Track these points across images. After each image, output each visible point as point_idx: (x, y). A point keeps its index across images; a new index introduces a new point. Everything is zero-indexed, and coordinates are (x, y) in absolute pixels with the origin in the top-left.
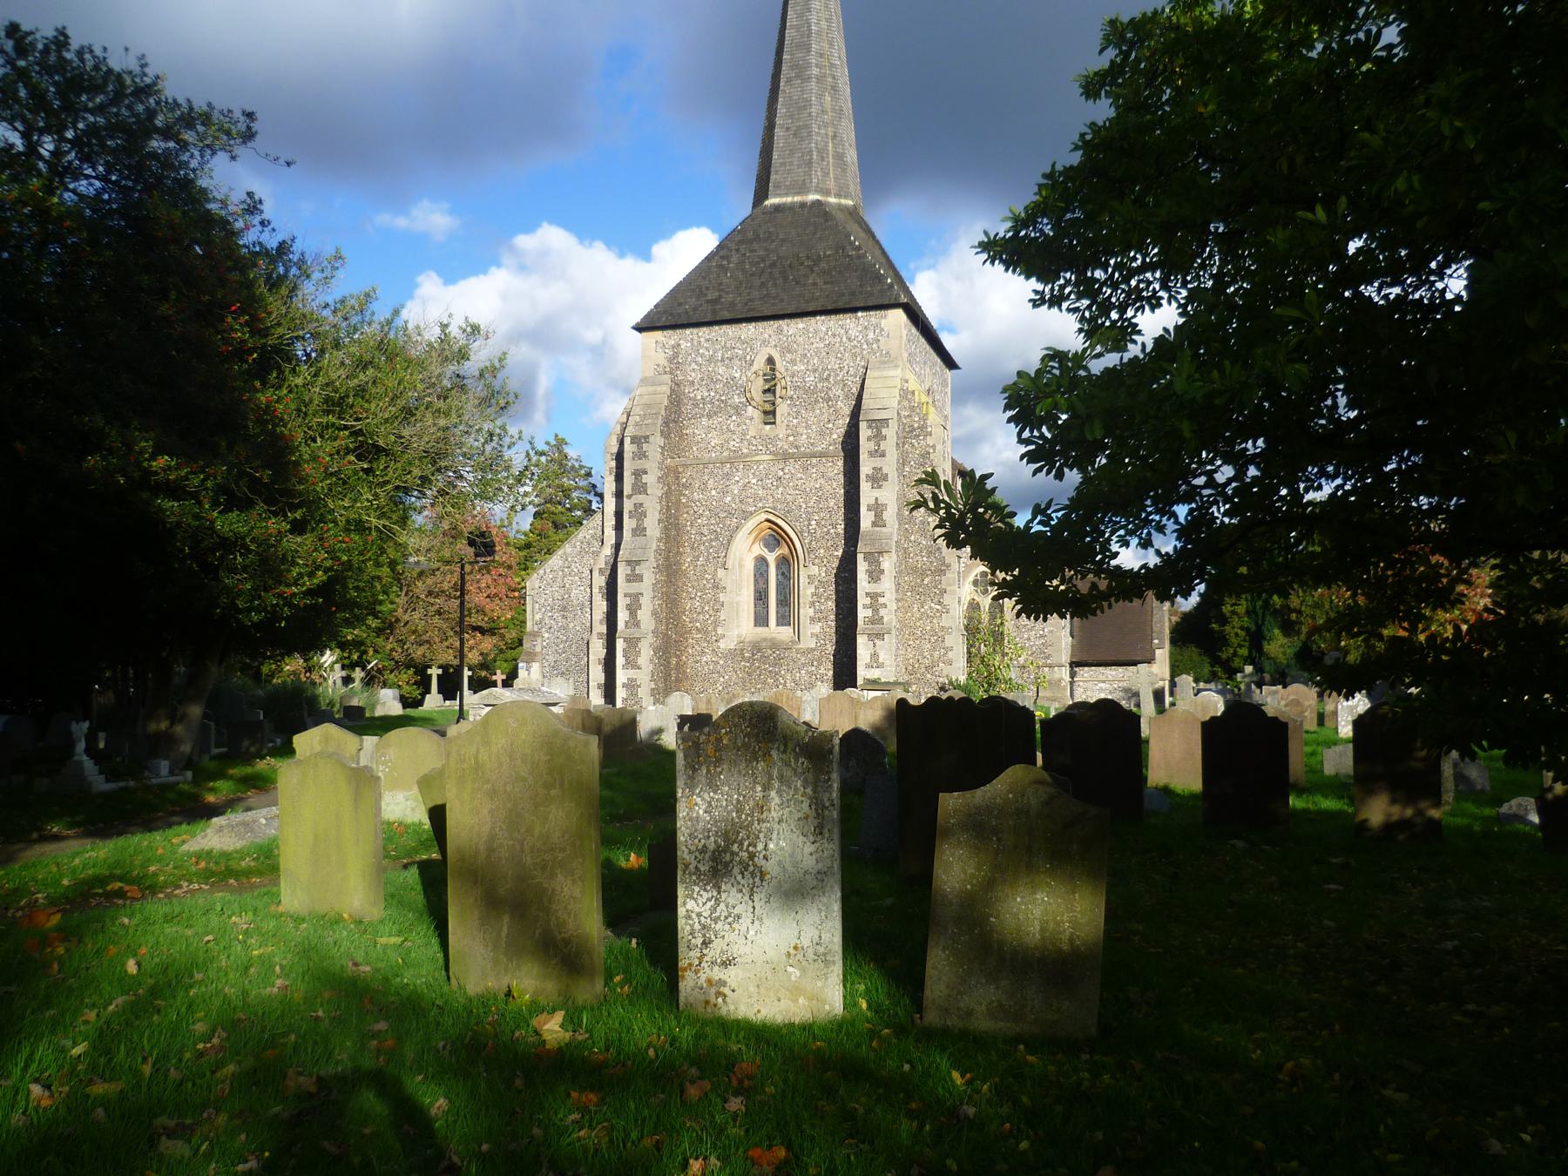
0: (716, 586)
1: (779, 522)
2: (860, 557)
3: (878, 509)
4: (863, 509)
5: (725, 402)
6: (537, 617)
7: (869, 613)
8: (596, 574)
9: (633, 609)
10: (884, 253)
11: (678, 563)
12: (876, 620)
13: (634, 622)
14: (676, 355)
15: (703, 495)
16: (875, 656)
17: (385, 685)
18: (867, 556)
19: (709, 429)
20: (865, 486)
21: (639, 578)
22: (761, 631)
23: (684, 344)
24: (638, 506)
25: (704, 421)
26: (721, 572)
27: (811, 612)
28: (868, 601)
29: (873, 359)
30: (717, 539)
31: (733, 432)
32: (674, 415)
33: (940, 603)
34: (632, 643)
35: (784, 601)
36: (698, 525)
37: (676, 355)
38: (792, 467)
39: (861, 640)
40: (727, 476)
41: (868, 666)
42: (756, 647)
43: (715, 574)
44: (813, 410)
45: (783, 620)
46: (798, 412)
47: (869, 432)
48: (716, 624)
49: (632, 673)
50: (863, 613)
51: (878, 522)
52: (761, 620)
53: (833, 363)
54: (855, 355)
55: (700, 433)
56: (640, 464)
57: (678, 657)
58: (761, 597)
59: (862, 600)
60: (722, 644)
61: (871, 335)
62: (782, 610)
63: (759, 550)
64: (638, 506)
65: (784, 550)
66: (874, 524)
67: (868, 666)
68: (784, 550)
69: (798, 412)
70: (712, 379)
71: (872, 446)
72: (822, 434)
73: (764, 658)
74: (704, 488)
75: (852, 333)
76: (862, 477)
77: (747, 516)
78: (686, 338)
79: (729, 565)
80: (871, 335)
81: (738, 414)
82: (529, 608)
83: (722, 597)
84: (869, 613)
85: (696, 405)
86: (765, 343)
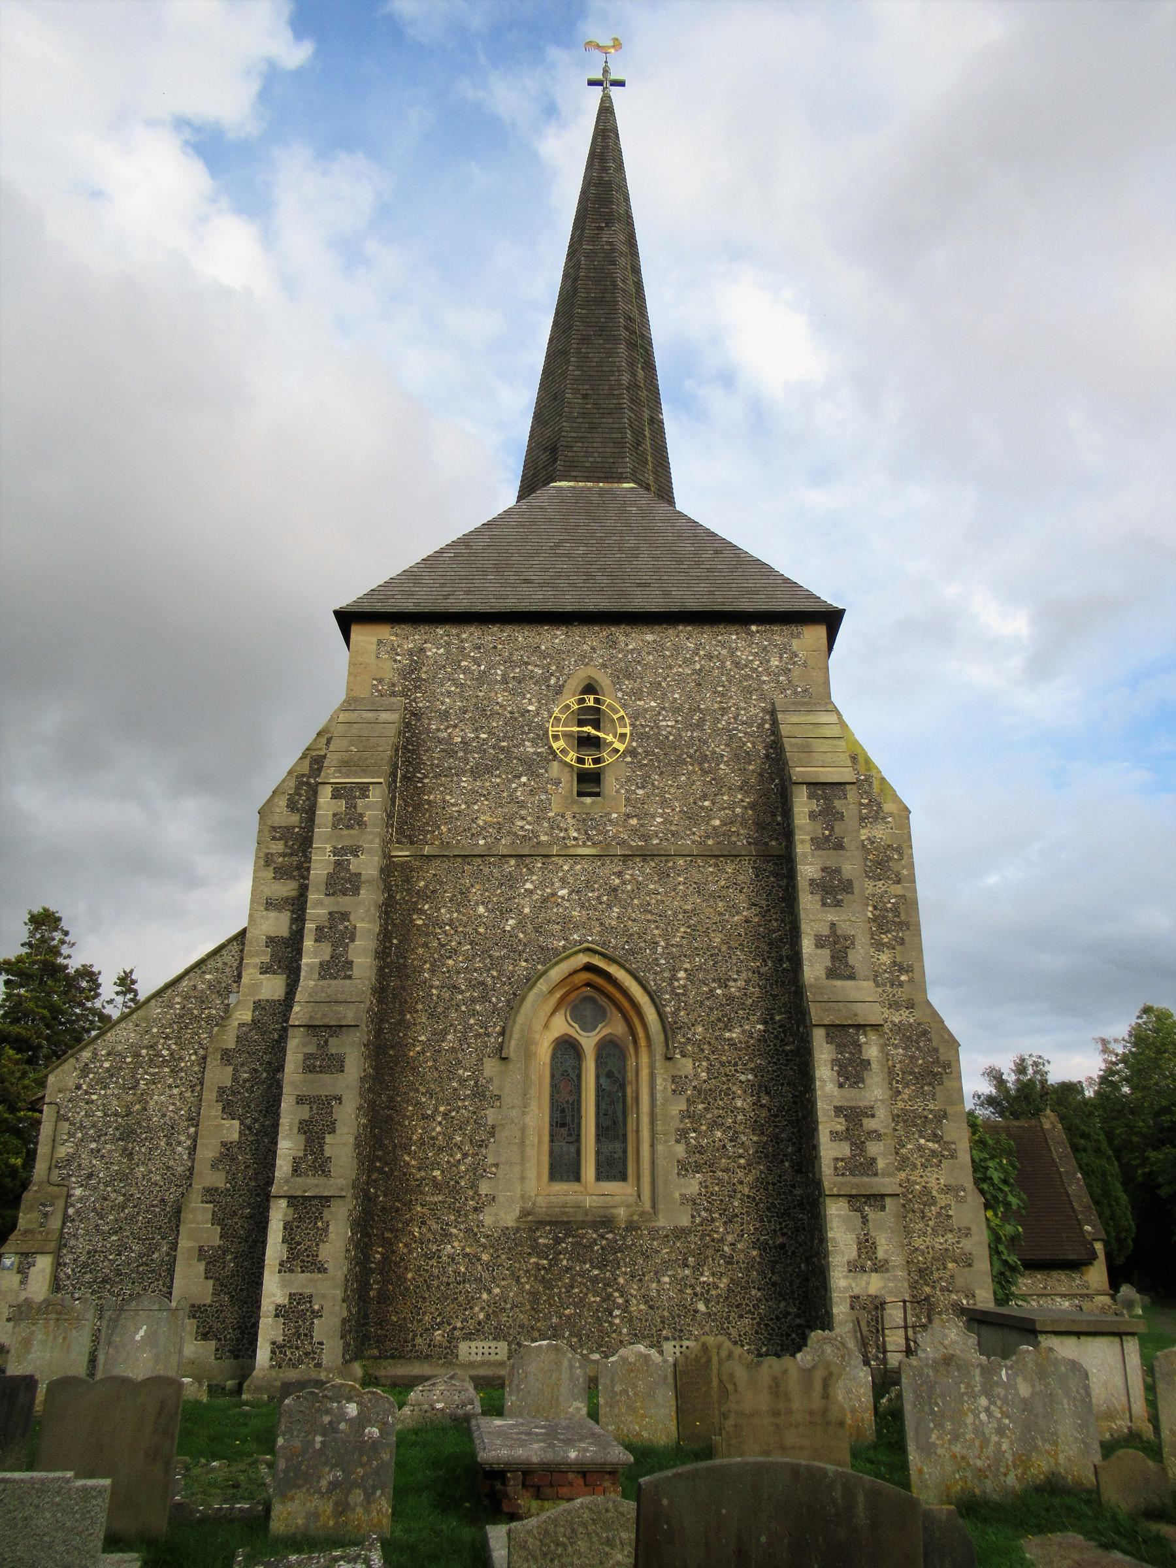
0: (479, 1093)
1: (613, 970)
2: (819, 1035)
3: (837, 945)
4: (807, 945)
5: (507, 751)
6: (63, 1151)
7: (845, 1149)
8: (214, 1063)
9: (314, 1133)
10: (187, 972)
11: (402, 1046)
12: (862, 1165)
13: (314, 1159)
14: (414, 667)
15: (463, 914)
16: (866, 1245)
17: (680, 1233)
18: (836, 1031)
19: (474, 796)
20: (808, 902)
21: (336, 1064)
22: (563, 1189)
23: (431, 651)
24: (339, 917)
25: (465, 782)
26: (490, 1067)
27: (680, 1150)
28: (840, 1125)
29: (779, 698)
30: (484, 998)
31: (522, 805)
32: (410, 763)
33: (935, 1138)
34: (308, 1209)
35: (613, 1128)
36: (449, 968)
37: (414, 667)
38: (636, 872)
39: (836, 1213)
40: (511, 881)
41: (855, 1268)
42: (562, 1225)
43: (478, 1069)
44: (676, 776)
45: (613, 1167)
46: (646, 778)
47: (814, 806)
48: (478, 1172)
49: (302, 1281)
50: (830, 1150)
51: (840, 969)
52: (564, 1167)
53: (708, 701)
54: (748, 691)
55: (456, 803)
56: (349, 837)
57: (388, 1244)
58: (564, 1120)
59: (827, 1125)
60: (487, 1217)
61: (775, 662)
62: (608, 1148)
63: (561, 1025)
64: (339, 917)
65: (615, 1027)
66: (832, 974)
67: (855, 1268)
68: (615, 1027)
69: (646, 778)
70: (483, 712)
71: (819, 829)
72: (691, 817)
73: (581, 1251)
74: (462, 899)
75: (743, 656)
76: (802, 883)
77: (552, 957)
78: (436, 644)
79: (512, 1049)
80: (775, 662)
81: (533, 774)
82: (46, 1130)
83: (491, 1116)
84: (845, 1149)
85: (452, 754)
86: (584, 659)
